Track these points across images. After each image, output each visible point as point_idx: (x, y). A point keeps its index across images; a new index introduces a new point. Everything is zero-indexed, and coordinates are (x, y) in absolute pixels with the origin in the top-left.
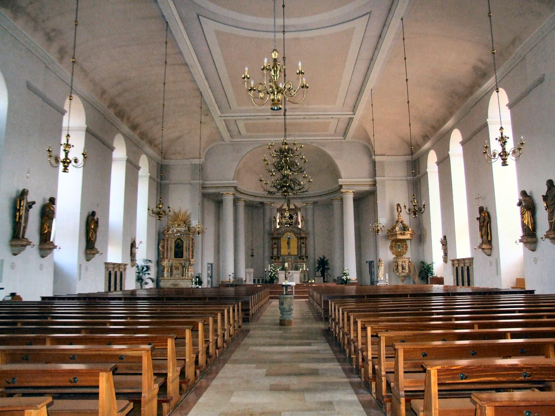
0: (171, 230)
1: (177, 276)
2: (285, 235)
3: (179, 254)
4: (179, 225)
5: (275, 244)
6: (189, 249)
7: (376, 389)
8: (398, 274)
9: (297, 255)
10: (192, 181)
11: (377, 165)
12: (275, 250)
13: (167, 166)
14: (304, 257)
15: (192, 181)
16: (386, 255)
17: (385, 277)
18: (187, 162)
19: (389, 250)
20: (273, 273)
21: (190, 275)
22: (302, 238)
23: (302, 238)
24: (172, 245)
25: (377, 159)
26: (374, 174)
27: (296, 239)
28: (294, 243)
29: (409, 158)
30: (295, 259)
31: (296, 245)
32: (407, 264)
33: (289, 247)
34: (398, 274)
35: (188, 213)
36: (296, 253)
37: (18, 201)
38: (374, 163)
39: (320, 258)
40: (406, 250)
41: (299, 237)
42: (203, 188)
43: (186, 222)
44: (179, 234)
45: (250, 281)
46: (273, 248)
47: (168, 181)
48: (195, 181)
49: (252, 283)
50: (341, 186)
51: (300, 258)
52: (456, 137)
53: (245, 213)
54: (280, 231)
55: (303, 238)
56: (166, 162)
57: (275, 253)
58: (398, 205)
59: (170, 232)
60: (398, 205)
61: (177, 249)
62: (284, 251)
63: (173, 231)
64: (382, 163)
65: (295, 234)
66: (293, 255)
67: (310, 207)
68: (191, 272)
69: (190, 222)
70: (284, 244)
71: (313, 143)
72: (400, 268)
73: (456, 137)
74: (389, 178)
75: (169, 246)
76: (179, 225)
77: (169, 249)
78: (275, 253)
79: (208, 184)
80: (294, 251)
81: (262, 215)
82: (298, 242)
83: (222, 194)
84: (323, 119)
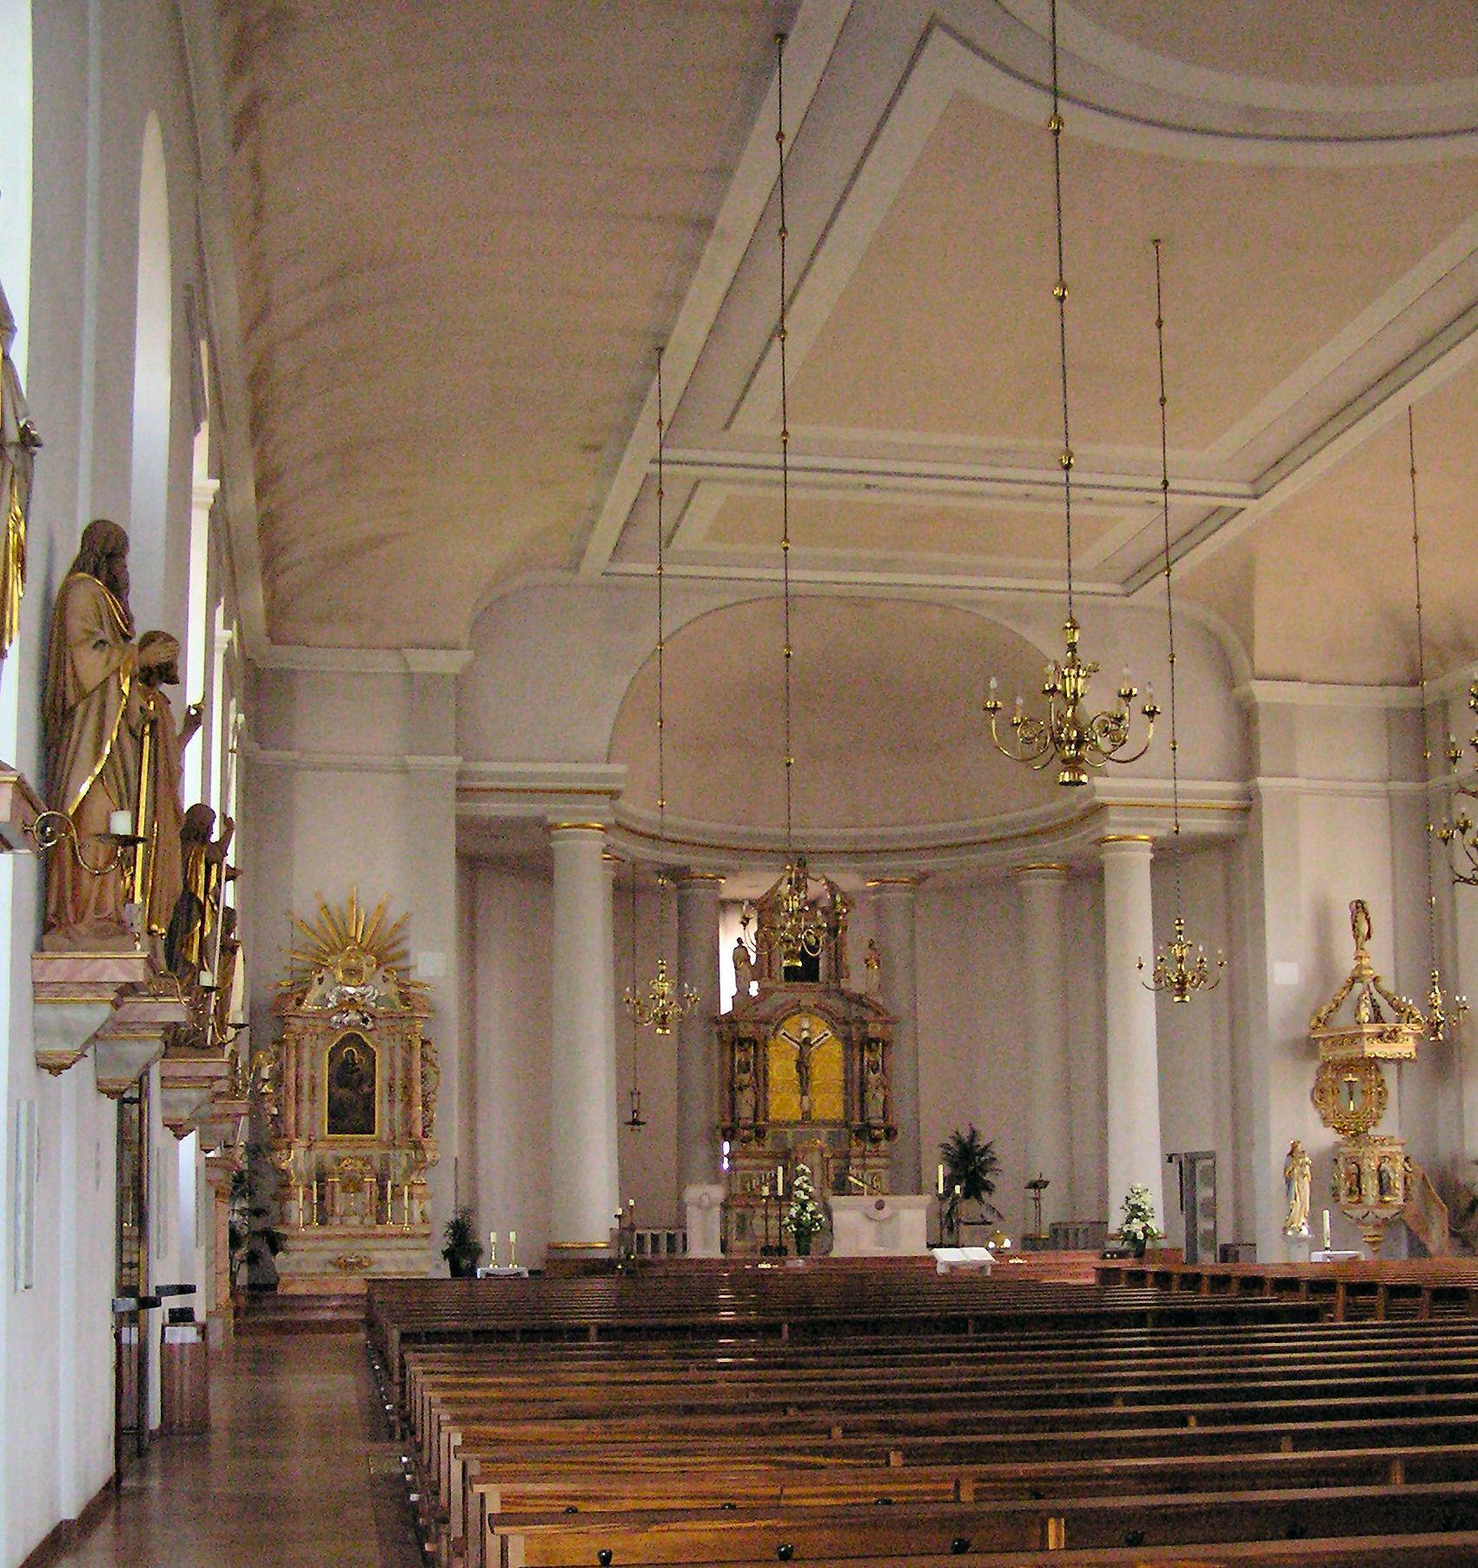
0: (313, 996)
1: (355, 1220)
2: (790, 1027)
3: (351, 1111)
4: (351, 972)
6: (407, 1088)
8: (1358, 1212)
10: (410, 759)
11: (1264, 724)
13: (285, 677)
15: (410, 759)
16: (1293, 1121)
17: (1314, 1221)
18: (386, 663)
19: (1310, 1105)
20: (810, 1208)
21: (417, 1218)
22: (867, 1039)
23: (868, 1043)
24: (315, 1067)
25: (1263, 692)
26: (1246, 765)
27: (837, 1049)
28: (829, 1061)
30: (834, 1139)
32: (1399, 1168)
34: (1358, 1212)
35: (395, 914)
37: (203, 867)
38: (1246, 716)
39: (959, 1142)
40: (1381, 1105)
42: (463, 793)
43: (386, 953)
44: (354, 1017)
45: (706, 1243)
46: (733, 1088)
47: (296, 755)
48: (439, 760)
49: (717, 1254)
50: (1099, 809)
51: (864, 1132)
54: (765, 1010)
55: (876, 1041)
56: (286, 657)
57: (746, 1111)
58: (1359, 907)
59: (308, 1006)
60: (1359, 907)
61: (343, 1093)
62: (784, 1103)
63: (324, 1000)
64: (1285, 713)
65: (835, 1021)
66: (824, 1123)
67: (897, 897)
68: (431, 1204)
69: (405, 955)
70: (781, 1067)
71: (977, 603)
72: (1370, 1186)
74: (1313, 784)
75: (306, 1071)
76: (351, 972)
77: (306, 1089)
78: (746, 1111)
79: (481, 776)
80: (829, 1104)
81: (673, 927)
82: (848, 1059)
83: (555, 826)
84: (943, 492)
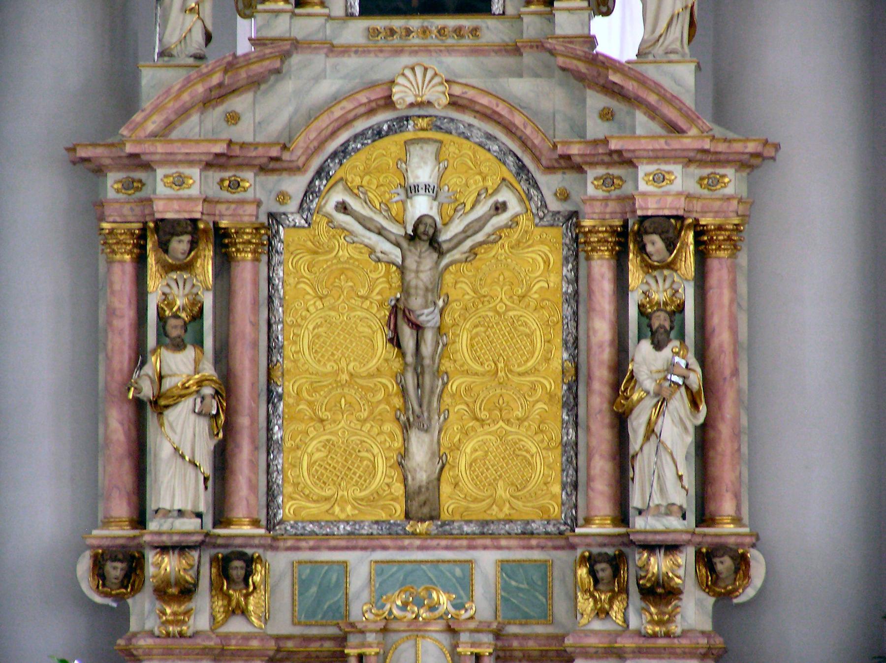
5: (183, 331)
7: (97, 359)
9: (562, 537)
12: (183, 434)
14: (680, 568)
27: (541, 260)
28: (514, 307)
29: (173, 580)
31: (543, 361)
33: (418, 397)
36: (542, 491)
41: (597, 209)
52: (114, 605)
53: (220, 528)
55: (670, 227)
57: (179, 490)
65: (532, 159)
66: (486, 532)
70: (324, 319)
73: (114, 605)
78: (179, 490)
